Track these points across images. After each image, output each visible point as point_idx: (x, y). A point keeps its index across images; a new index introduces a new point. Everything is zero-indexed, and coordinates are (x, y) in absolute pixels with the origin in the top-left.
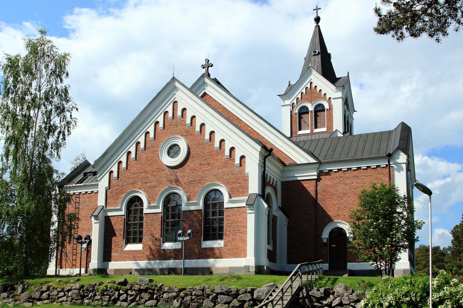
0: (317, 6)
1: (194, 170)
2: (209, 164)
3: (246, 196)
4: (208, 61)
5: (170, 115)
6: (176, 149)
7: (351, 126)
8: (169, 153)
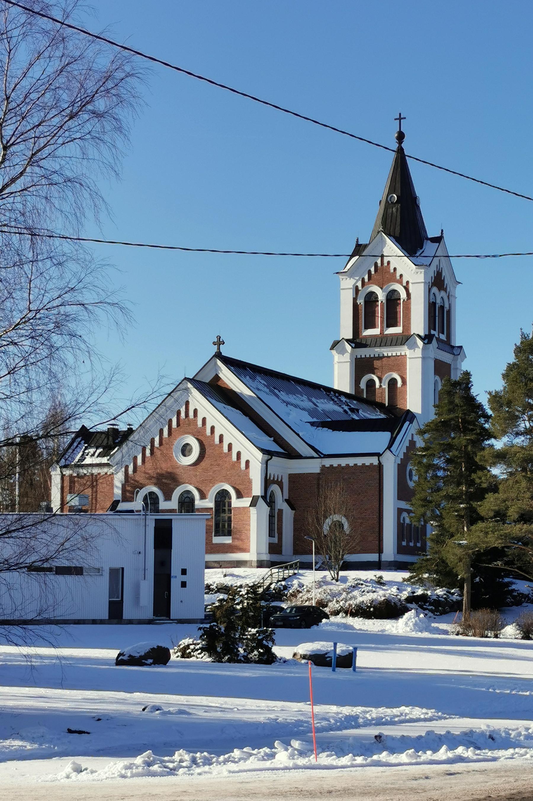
0: (400, 114)
1: (206, 470)
2: (219, 465)
3: (251, 497)
4: (220, 337)
5: (183, 415)
6: (188, 447)
7: (449, 312)
8: (184, 455)
